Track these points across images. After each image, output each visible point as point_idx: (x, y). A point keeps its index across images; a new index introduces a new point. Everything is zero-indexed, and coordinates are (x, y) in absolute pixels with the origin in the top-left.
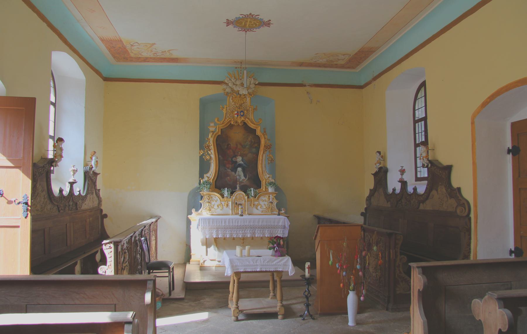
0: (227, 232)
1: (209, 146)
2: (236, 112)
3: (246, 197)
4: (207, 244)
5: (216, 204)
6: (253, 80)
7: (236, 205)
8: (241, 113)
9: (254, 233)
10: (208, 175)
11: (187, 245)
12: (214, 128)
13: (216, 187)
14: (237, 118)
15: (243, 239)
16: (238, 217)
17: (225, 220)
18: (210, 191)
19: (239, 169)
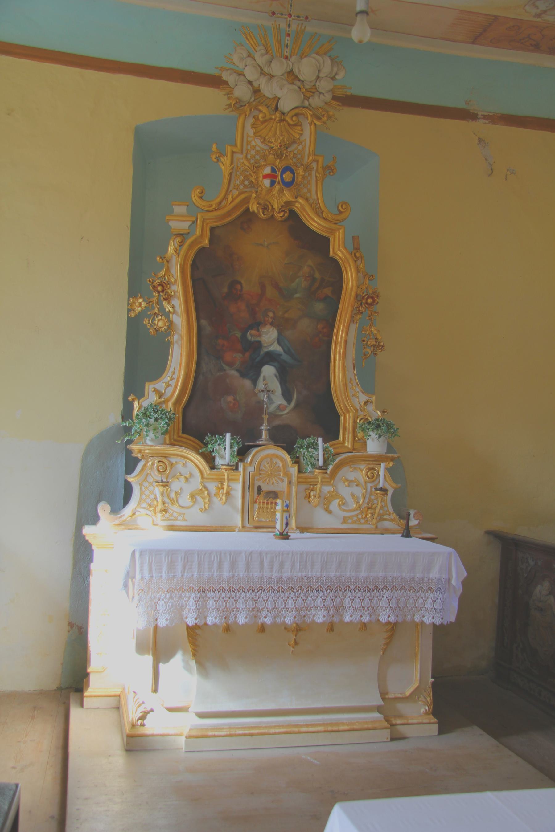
0: (240, 605)
1: (165, 285)
2: (267, 170)
3: (294, 470)
4: (158, 646)
5: (189, 489)
6: (328, 62)
7: (261, 495)
8: (286, 175)
9: (339, 608)
10: (160, 385)
11: (71, 625)
12: (185, 221)
13: (187, 429)
14: (270, 191)
15: (298, 629)
16: (264, 541)
17: (234, 557)
18: (165, 444)
19: (269, 371)
